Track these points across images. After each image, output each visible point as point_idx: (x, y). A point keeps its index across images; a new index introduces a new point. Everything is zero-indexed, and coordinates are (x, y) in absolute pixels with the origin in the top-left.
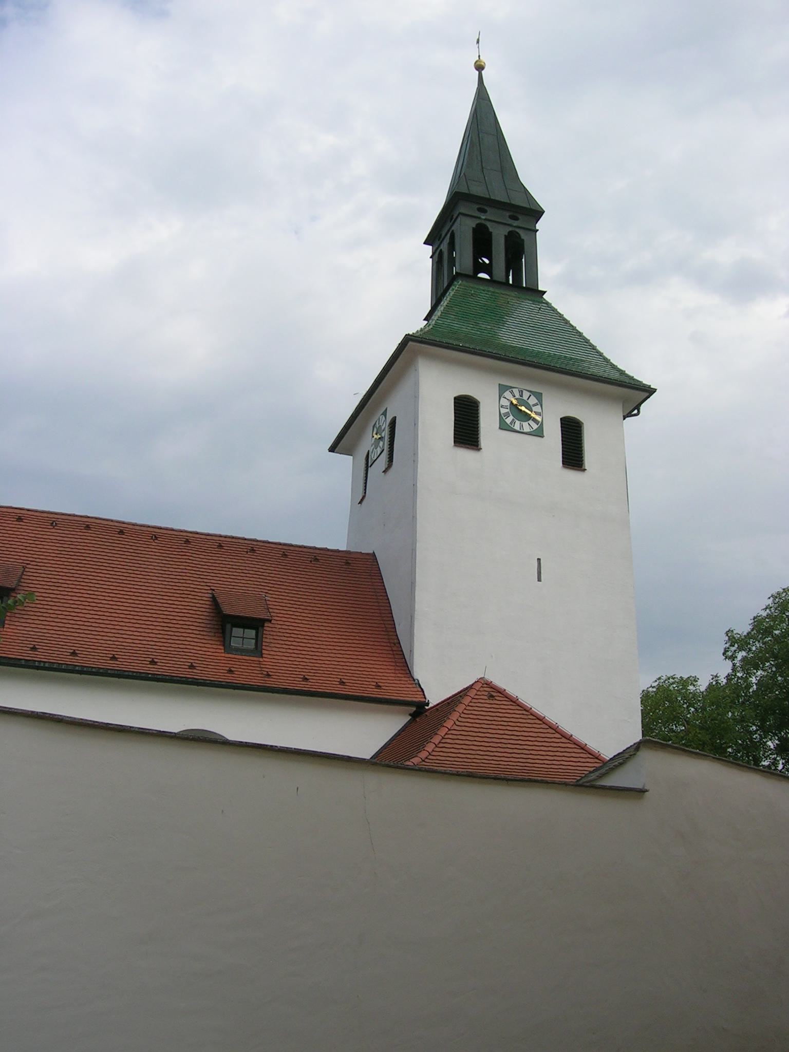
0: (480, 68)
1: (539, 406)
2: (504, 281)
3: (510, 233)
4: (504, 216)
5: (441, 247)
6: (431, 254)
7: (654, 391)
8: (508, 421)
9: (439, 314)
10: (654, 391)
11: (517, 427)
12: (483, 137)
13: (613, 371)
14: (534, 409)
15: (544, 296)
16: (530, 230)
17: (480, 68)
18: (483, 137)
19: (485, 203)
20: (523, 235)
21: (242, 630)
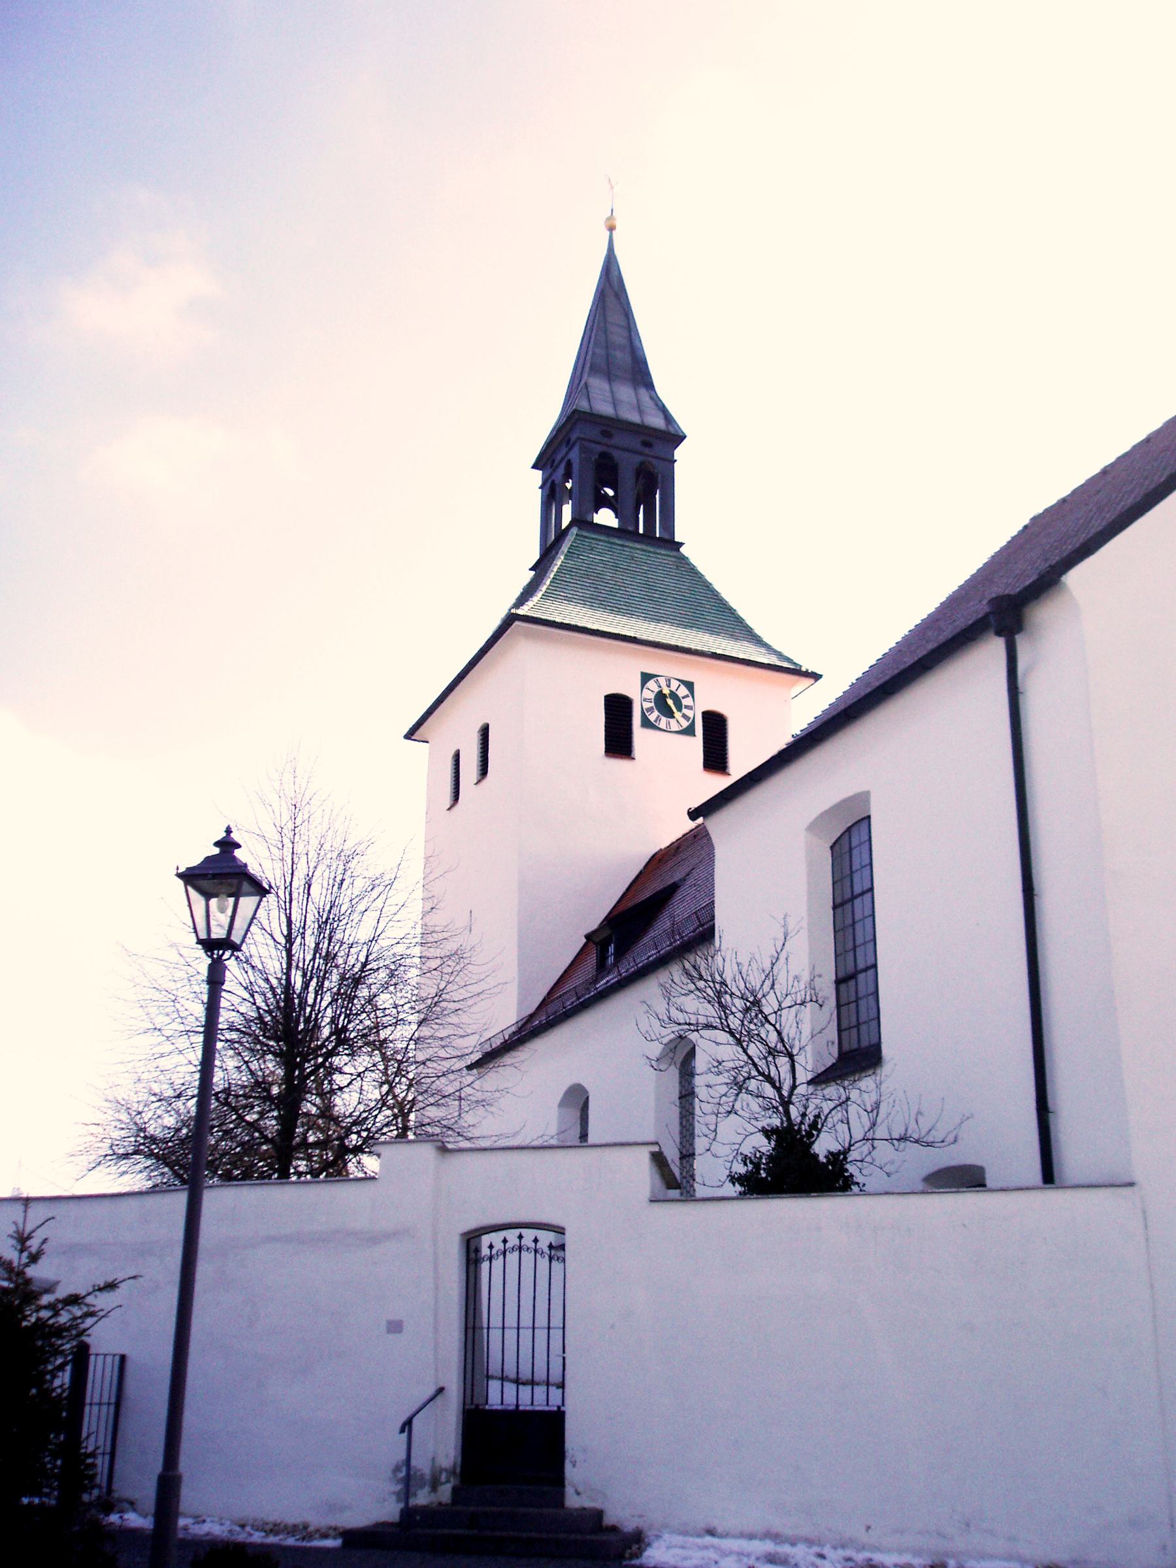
0: (611, 229)
1: (690, 699)
2: (521, 1387)
3: (642, 463)
4: (635, 443)
5: (553, 477)
6: (540, 483)
7: (821, 676)
8: (652, 717)
9: (548, 582)
10: (821, 676)
11: (662, 725)
12: (612, 340)
13: (652, 954)
14: (685, 711)
15: (682, 550)
16: (664, 460)
17: (611, 229)
18: (612, 340)
19: (610, 426)
20: (659, 466)
21: (697, 1140)
